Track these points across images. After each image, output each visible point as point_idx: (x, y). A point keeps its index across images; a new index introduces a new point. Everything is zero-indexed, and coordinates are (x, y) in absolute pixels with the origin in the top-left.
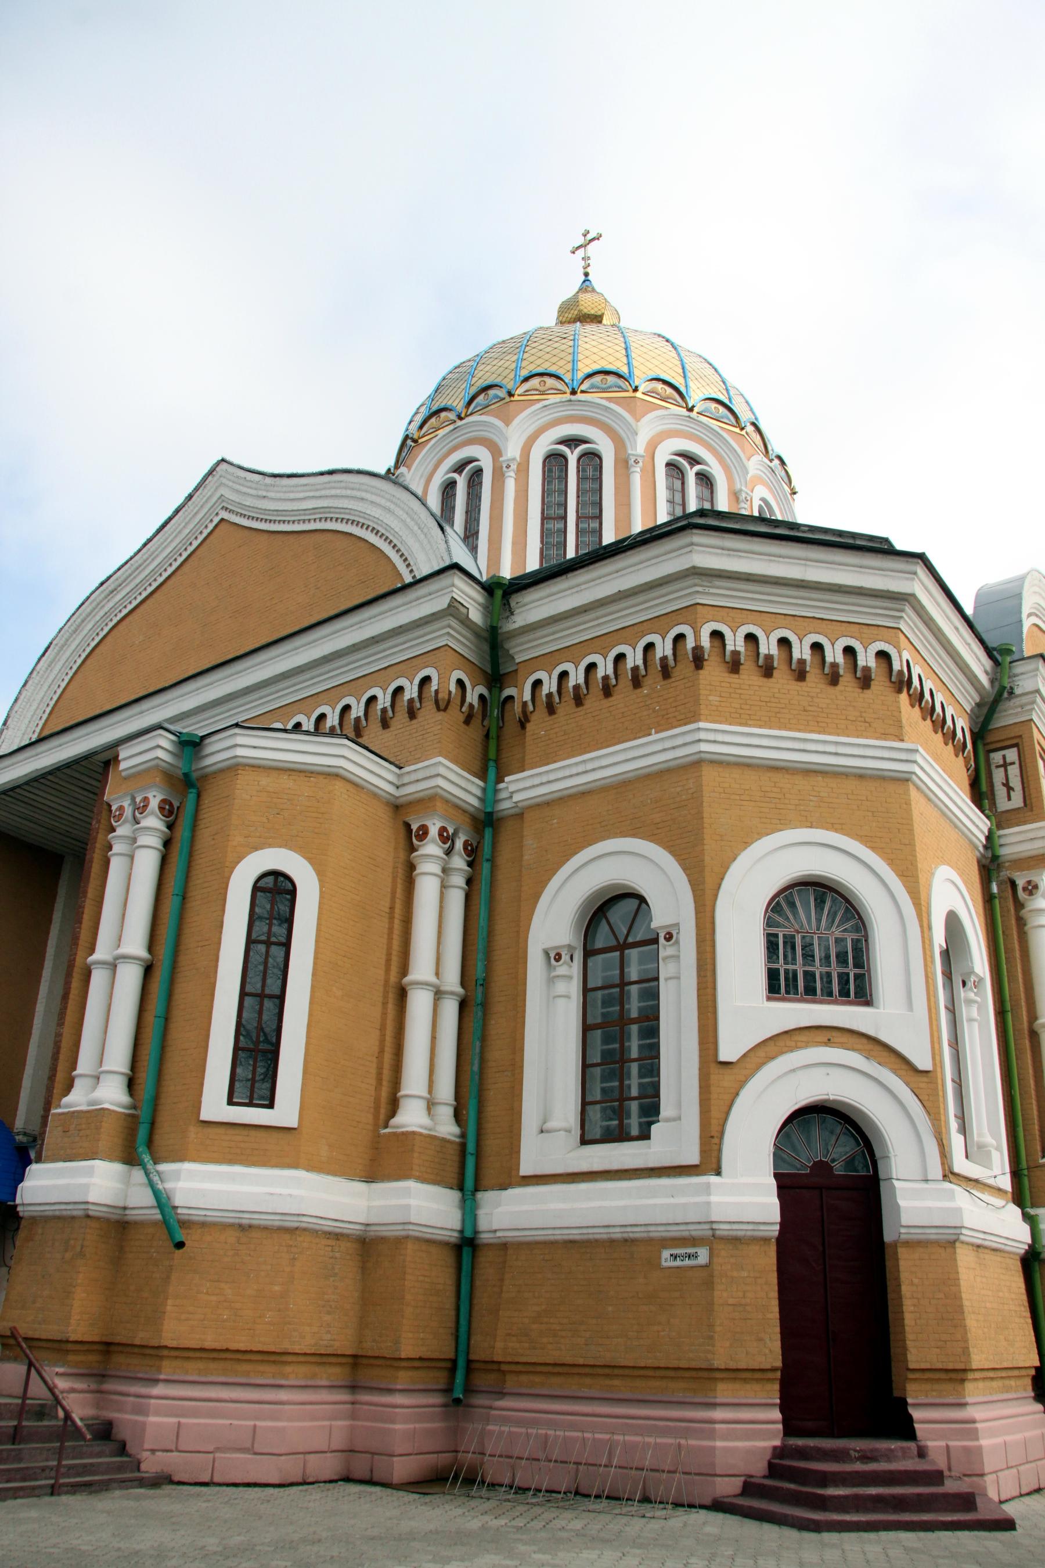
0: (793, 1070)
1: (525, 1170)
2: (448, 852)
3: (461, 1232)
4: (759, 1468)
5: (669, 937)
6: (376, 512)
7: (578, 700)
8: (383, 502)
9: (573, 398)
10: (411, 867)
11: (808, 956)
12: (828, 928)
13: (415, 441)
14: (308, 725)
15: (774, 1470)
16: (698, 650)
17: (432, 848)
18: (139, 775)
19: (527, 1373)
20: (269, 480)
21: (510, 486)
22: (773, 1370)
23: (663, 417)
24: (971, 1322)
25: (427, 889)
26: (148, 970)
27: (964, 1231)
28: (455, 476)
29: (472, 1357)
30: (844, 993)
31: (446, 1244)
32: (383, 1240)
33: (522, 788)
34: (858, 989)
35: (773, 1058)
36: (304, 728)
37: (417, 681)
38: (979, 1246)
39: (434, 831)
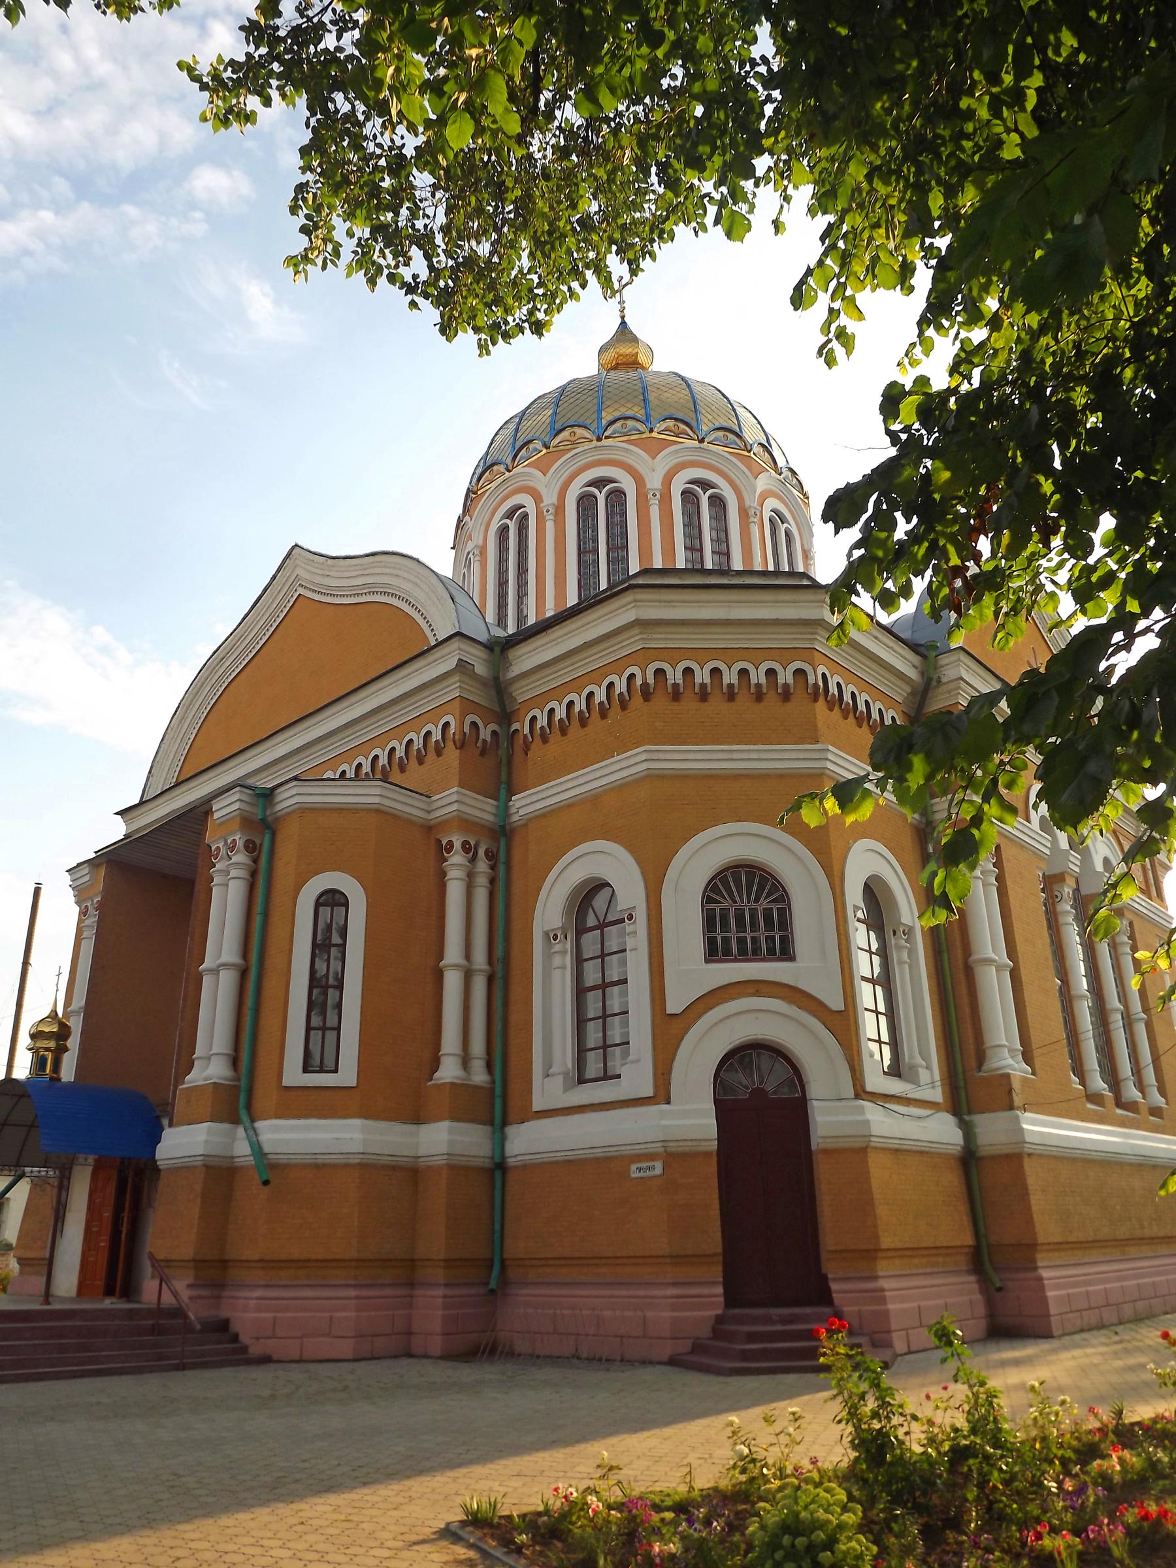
0: (728, 1017)
1: (536, 1107)
2: (473, 860)
3: (492, 1158)
4: (705, 1332)
5: (630, 917)
6: (406, 586)
7: (564, 731)
8: (412, 578)
9: (599, 444)
10: (443, 874)
11: (740, 925)
12: (757, 901)
13: (475, 493)
14: (351, 774)
15: (717, 1334)
16: (645, 685)
17: (457, 858)
18: (225, 822)
19: (542, 1266)
20: (330, 562)
21: (550, 526)
22: (715, 1255)
23: (676, 451)
24: (882, 1212)
25: (455, 892)
26: (244, 973)
27: (873, 1139)
28: (508, 521)
29: (505, 1256)
30: (771, 951)
31: (482, 1169)
32: (430, 1168)
33: (524, 804)
34: (785, 951)
35: (711, 1008)
36: (348, 776)
37: (440, 726)
38: (897, 1150)
39: (457, 845)
